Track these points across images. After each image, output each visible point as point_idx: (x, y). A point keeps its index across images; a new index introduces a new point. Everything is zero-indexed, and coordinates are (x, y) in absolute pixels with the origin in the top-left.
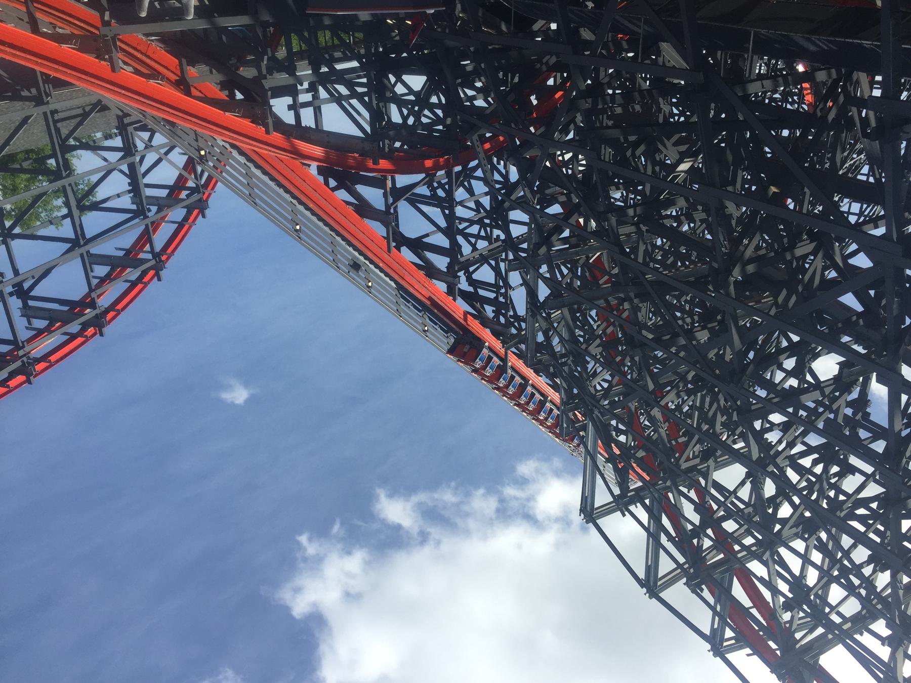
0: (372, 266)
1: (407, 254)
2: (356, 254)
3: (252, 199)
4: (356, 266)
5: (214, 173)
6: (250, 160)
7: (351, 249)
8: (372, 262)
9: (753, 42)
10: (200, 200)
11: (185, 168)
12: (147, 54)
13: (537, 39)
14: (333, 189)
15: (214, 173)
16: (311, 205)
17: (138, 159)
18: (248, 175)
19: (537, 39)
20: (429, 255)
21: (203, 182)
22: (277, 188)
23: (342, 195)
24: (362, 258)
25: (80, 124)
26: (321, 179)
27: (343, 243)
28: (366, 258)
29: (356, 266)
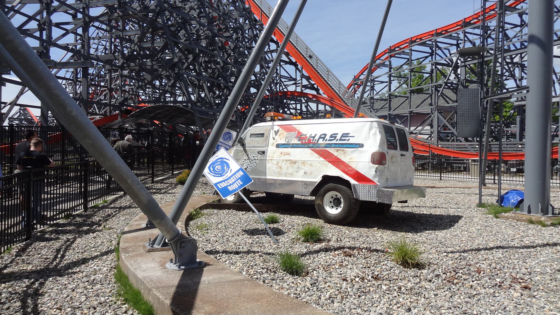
0: (305, 56)
1: (294, 60)
2: (310, 61)
3: (340, 83)
4: (310, 57)
5: (347, 90)
6: (342, 99)
7: (312, 63)
8: (305, 57)
9: (400, 146)
10: (355, 81)
11: (357, 91)
12: (482, 197)
13: (155, 121)
14: (315, 84)
15: (347, 90)
16: (322, 79)
17: (369, 96)
18: (328, 78)
19: (155, 121)
20: (287, 60)
21: (353, 86)
22: (332, 86)
23: (313, 82)
24: (308, 60)
25: (383, 106)
26: (319, 88)
27: (314, 66)
28: (307, 59)
29: (310, 57)
